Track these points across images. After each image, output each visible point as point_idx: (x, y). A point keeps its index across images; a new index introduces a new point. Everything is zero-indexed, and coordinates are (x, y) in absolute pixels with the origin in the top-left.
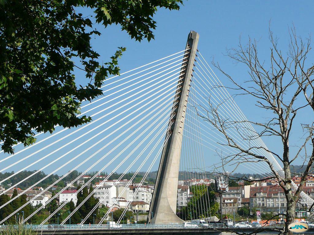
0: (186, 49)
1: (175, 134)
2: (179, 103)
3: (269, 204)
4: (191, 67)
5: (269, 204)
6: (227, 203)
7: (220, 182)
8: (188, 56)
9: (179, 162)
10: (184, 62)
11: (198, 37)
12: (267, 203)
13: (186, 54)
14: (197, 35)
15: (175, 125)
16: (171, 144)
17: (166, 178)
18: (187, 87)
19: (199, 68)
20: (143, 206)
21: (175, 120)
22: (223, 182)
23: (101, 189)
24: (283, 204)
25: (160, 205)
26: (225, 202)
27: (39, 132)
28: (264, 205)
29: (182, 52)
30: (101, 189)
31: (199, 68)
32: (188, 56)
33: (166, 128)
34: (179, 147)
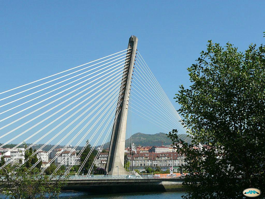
0: (128, 49)
1: (124, 109)
2: (126, 87)
3: (149, 164)
4: (133, 61)
5: (149, 164)
6: (103, 164)
7: (132, 147)
8: (131, 53)
9: (126, 131)
10: (127, 58)
11: (137, 40)
12: (174, 163)
13: (128, 52)
14: (137, 38)
15: (124, 103)
16: (121, 117)
17: (119, 141)
18: (130, 76)
19: (138, 62)
20: (46, 165)
21: (123, 100)
22: (134, 147)
23: (17, 153)
24: (142, 164)
25: (115, 161)
26: (103, 163)
27: (182, 99)
28: (142, 165)
29: (125, 51)
30: (17, 153)
31: (138, 62)
32: (131, 53)
33: (115, 107)
34: (125, 120)
